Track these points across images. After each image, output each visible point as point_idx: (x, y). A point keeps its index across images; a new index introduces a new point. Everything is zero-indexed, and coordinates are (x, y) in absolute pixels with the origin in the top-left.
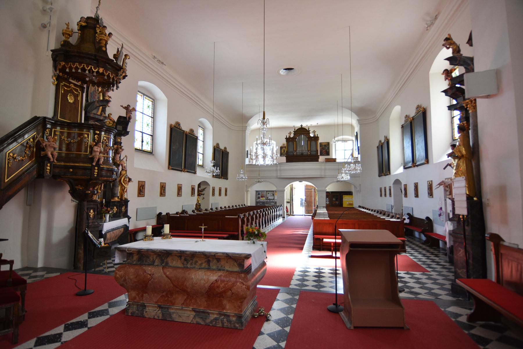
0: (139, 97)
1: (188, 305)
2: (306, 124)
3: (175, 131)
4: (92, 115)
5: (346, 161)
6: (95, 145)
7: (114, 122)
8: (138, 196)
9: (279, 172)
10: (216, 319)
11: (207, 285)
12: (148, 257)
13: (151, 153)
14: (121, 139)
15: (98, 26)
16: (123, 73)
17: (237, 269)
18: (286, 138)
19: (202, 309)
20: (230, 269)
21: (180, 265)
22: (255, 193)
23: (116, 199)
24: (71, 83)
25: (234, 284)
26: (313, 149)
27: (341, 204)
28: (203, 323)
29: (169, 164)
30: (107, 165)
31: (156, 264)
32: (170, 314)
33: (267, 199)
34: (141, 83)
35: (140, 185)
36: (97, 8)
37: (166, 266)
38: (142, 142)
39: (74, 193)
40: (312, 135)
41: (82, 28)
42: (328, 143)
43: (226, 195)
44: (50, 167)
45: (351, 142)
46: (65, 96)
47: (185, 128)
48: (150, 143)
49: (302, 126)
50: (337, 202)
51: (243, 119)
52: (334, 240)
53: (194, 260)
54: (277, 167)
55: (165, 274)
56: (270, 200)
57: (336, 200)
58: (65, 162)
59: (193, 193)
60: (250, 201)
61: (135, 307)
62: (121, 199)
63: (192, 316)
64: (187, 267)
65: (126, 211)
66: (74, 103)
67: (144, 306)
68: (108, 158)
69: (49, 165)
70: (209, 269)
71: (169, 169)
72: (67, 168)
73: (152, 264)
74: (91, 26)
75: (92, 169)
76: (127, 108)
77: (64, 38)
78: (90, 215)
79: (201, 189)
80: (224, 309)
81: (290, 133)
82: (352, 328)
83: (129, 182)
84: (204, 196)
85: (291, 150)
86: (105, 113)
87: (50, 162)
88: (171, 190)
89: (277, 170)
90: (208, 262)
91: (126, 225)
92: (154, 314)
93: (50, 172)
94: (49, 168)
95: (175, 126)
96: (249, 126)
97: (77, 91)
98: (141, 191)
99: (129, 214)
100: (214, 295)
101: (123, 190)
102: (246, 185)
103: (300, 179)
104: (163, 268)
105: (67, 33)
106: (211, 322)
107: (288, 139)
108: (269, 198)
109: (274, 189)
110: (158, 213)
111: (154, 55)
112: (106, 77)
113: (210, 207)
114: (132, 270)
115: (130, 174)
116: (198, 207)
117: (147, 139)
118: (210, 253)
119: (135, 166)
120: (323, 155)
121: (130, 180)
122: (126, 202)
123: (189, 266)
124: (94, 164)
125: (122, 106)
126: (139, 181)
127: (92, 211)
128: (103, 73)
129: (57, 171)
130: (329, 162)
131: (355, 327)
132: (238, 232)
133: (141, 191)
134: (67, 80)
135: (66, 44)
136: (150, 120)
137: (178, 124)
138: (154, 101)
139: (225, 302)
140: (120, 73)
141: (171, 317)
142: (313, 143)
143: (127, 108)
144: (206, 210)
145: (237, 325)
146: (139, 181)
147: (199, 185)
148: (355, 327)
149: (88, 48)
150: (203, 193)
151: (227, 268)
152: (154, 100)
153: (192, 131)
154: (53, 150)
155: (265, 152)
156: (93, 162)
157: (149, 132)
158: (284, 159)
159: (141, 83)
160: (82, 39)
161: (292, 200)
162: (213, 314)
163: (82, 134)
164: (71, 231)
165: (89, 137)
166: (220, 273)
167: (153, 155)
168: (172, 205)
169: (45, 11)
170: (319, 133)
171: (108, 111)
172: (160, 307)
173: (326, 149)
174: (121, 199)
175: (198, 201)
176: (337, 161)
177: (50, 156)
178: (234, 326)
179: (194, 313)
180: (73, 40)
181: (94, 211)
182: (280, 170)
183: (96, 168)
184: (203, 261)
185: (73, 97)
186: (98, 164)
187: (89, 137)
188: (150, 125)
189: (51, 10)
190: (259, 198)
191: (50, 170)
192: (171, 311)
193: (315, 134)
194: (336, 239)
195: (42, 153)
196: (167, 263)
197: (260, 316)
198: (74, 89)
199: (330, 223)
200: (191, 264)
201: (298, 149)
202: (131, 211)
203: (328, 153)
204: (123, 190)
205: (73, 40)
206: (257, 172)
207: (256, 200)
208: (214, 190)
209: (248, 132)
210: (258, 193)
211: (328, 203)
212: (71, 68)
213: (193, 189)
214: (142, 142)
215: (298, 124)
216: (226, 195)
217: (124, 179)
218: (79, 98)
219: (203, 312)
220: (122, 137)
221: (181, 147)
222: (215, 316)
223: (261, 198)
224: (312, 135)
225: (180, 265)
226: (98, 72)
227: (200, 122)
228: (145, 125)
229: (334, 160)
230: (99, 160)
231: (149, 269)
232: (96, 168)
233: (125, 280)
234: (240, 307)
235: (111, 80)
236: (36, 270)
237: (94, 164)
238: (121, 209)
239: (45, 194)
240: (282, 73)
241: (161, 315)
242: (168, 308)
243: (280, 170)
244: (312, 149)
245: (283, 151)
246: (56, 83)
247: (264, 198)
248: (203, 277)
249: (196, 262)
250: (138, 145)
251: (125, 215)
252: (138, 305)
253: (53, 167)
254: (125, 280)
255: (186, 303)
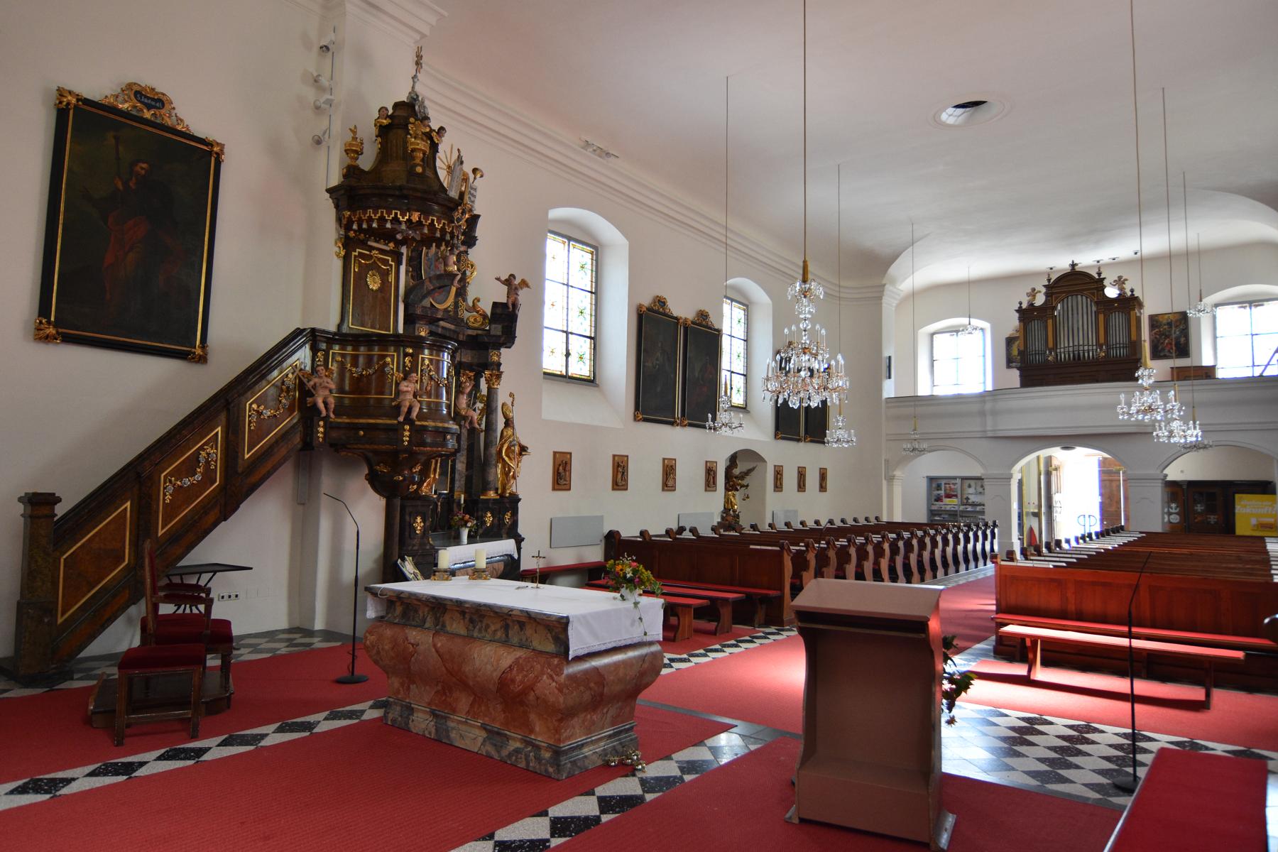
0: (554, 247)
1: (475, 716)
2: (1086, 259)
3: (653, 324)
4: (419, 312)
5: (1257, 372)
6: (405, 379)
7: (484, 316)
8: (554, 489)
9: (989, 420)
10: (517, 751)
11: (496, 675)
12: (416, 611)
13: (590, 382)
14: (499, 356)
15: (412, 120)
16: (463, 213)
17: (551, 648)
18: (1020, 310)
19: (497, 726)
20: (539, 648)
21: (463, 632)
22: (923, 485)
23: (492, 494)
24: (374, 248)
25: (537, 679)
26: (1118, 336)
27: (1228, 526)
28: (496, 756)
29: (637, 408)
30: (434, 420)
31: (427, 625)
32: (447, 731)
33: (966, 502)
34: (555, 213)
35: (558, 462)
36: (414, 77)
37: (440, 629)
38: (568, 355)
39: (378, 483)
40: (1111, 292)
41: (383, 131)
42: (1183, 318)
43: (823, 488)
44: (324, 427)
45: (978, 334)
46: (361, 278)
47: (682, 309)
48: (587, 356)
49: (1073, 265)
50: (1212, 519)
51: (868, 268)
52: (1124, 642)
53: (485, 621)
54: (984, 402)
55: (435, 646)
56: (974, 505)
57: (1211, 510)
58: (349, 416)
59: (710, 483)
60: (903, 501)
61: (398, 708)
62: (502, 496)
63: (480, 740)
64: (472, 637)
65: (515, 523)
66: (380, 290)
67: (411, 710)
68: (438, 405)
69: (321, 423)
70: (506, 642)
71: (636, 419)
72: (357, 427)
73: (421, 625)
74: (403, 121)
75: (397, 429)
76: (508, 282)
77: (348, 161)
78: (415, 529)
79: (738, 472)
80: (532, 731)
81: (1033, 293)
82: (796, 821)
83: (520, 454)
84: (749, 491)
85: (1037, 345)
86: (465, 300)
87: (323, 419)
88: (644, 473)
89: (982, 414)
90: (506, 628)
91: (511, 556)
92: (423, 726)
93: (324, 438)
94: (321, 430)
95: (649, 309)
96: (893, 282)
97: (385, 262)
98: (561, 474)
99: (521, 530)
100: (510, 698)
101: (507, 474)
102: (887, 461)
103: (1069, 441)
104: (436, 634)
105: (353, 151)
106: (510, 755)
107: (1027, 314)
108: (973, 499)
109: (977, 471)
110: (606, 532)
111: (584, 137)
112: (426, 231)
113: (769, 520)
114: (388, 632)
115: (523, 433)
116: (729, 518)
117: (581, 347)
118: (501, 608)
119: (545, 416)
120: (1165, 357)
121: (523, 449)
122: (515, 500)
123: (476, 634)
124: (401, 419)
125: (498, 279)
126: (555, 453)
127: (419, 520)
128: (420, 223)
129: (334, 434)
130: (1186, 378)
131: (802, 820)
132: (782, 589)
133: (561, 474)
134: (363, 244)
135: (352, 172)
136: (586, 301)
137: (661, 302)
138: (597, 250)
139: (533, 716)
140: (457, 215)
141: (448, 737)
142: (1117, 319)
143: (508, 282)
144: (754, 527)
145: (551, 770)
146: (555, 453)
147: (733, 460)
148: (802, 820)
149: (395, 173)
150: (745, 482)
151: (536, 644)
152: (596, 248)
153: (703, 315)
154: (327, 392)
155: (960, 362)
156: (399, 415)
157: (585, 326)
158: (1014, 376)
159: (555, 213)
160: (384, 155)
161: (1050, 507)
162: (514, 739)
163: (384, 357)
164: (376, 561)
165: (393, 361)
166: (520, 653)
167: (597, 386)
168: (645, 513)
169: (317, 108)
170: (1134, 285)
171: (472, 293)
172: (433, 713)
173: (1175, 336)
174: (502, 496)
175: (727, 501)
176: (1220, 374)
177: (321, 406)
178: (546, 770)
179: (484, 734)
180: (366, 162)
181: (424, 520)
182: (995, 413)
183: (407, 427)
184: (498, 626)
185: (378, 279)
186: (408, 420)
187: (393, 361)
188: (587, 311)
189: (329, 103)
190: (939, 499)
191: (324, 433)
192: (451, 724)
193: (1122, 289)
194: (1130, 636)
195: (309, 400)
196: (444, 626)
197: (622, 764)
198: (380, 259)
199: (1052, 580)
200: (480, 631)
201: (1064, 343)
202: (529, 519)
203: (1183, 349)
204: (508, 474)
205: (366, 162)
206: (927, 418)
207: (929, 504)
208: (778, 474)
209: (889, 303)
210: (934, 482)
211: (1175, 519)
212: (360, 222)
213: (710, 472)
214: (568, 355)
215: (1061, 262)
216: (823, 488)
217: (509, 448)
218: (392, 278)
219: (498, 734)
220: (503, 350)
221: (673, 363)
222: (518, 745)
223: (947, 501)
224: (1111, 292)
225: (463, 632)
226: (409, 220)
227: (735, 288)
228: (574, 314)
229: (1208, 373)
230: (410, 409)
231: (414, 635)
232: (407, 427)
233: (378, 652)
234: (557, 731)
235: (438, 235)
236: (310, 633)
237: (401, 419)
238: (503, 519)
239: (327, 481)
240: (951, 121)
241: (433, 730)
242: (446, 718)
243: (995, 413)
244: (1112, 341)
245: (1015, 352)
246: (343, 253)
247: (955, 501)
248: (491, 659)
249: (488, 626)
250: (552, 363)
251: (512, 532)
252: (402, 706)
253: (329, 426)
254: (378, 652)
255: (472, 713)
